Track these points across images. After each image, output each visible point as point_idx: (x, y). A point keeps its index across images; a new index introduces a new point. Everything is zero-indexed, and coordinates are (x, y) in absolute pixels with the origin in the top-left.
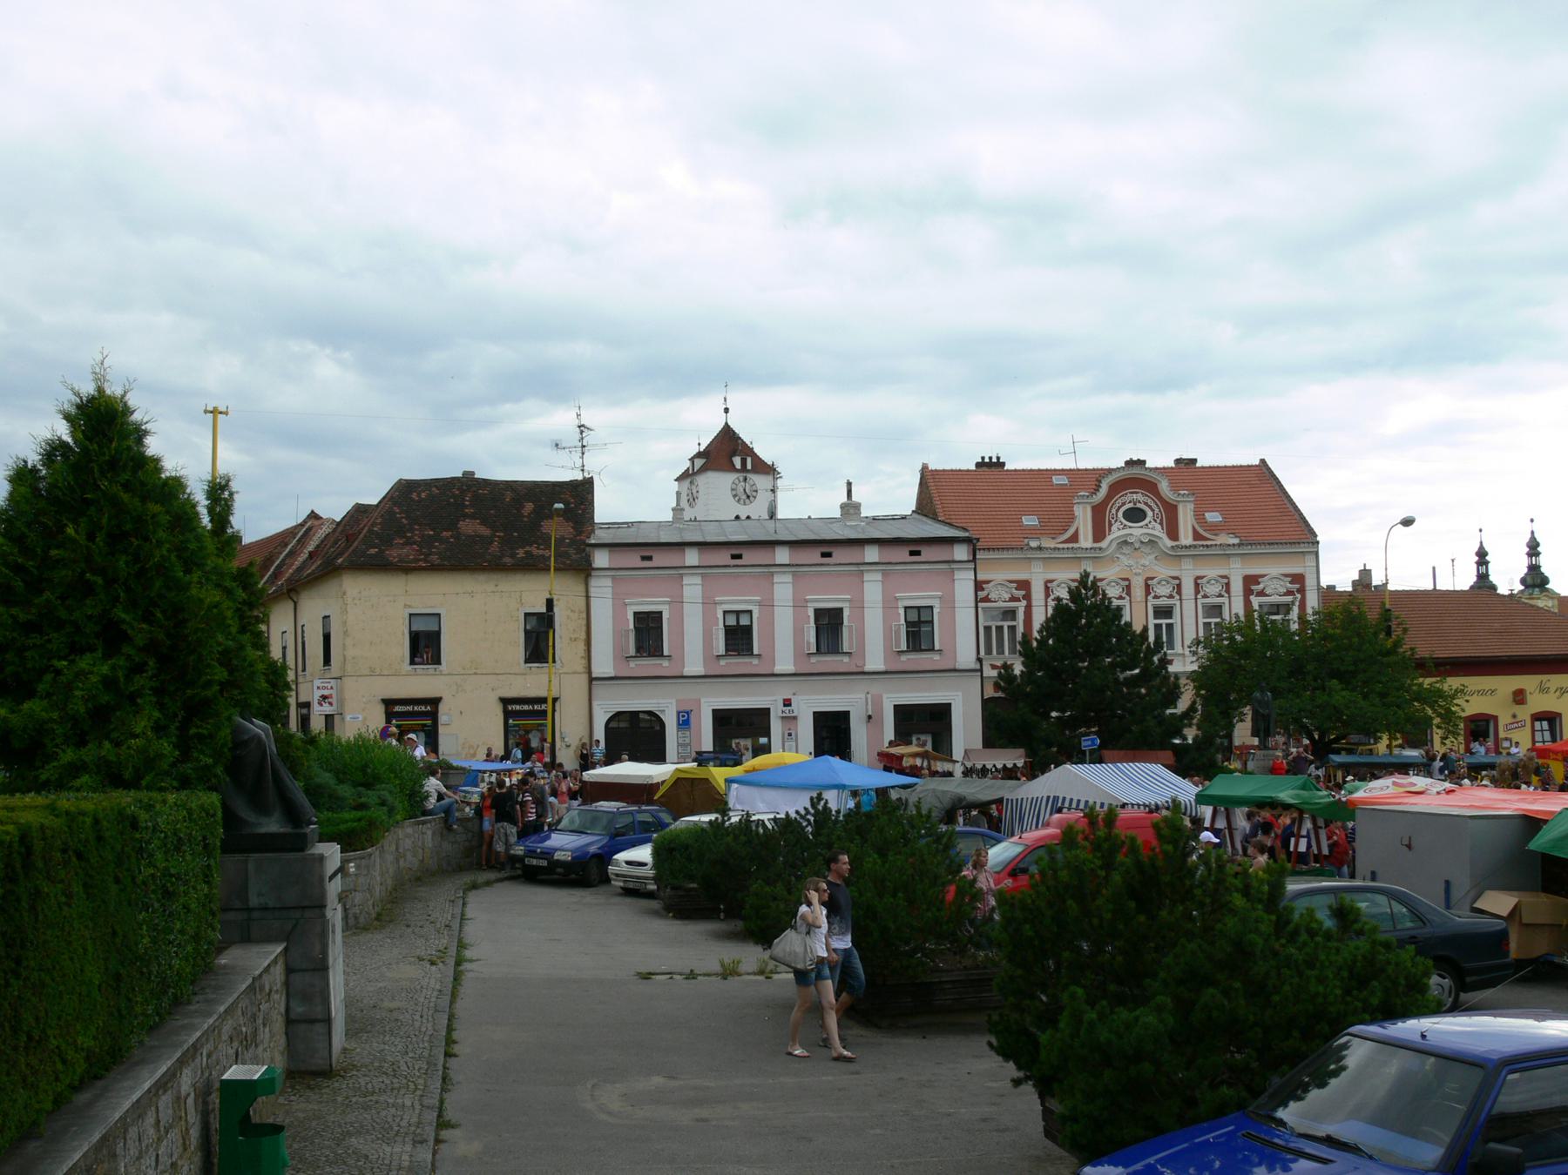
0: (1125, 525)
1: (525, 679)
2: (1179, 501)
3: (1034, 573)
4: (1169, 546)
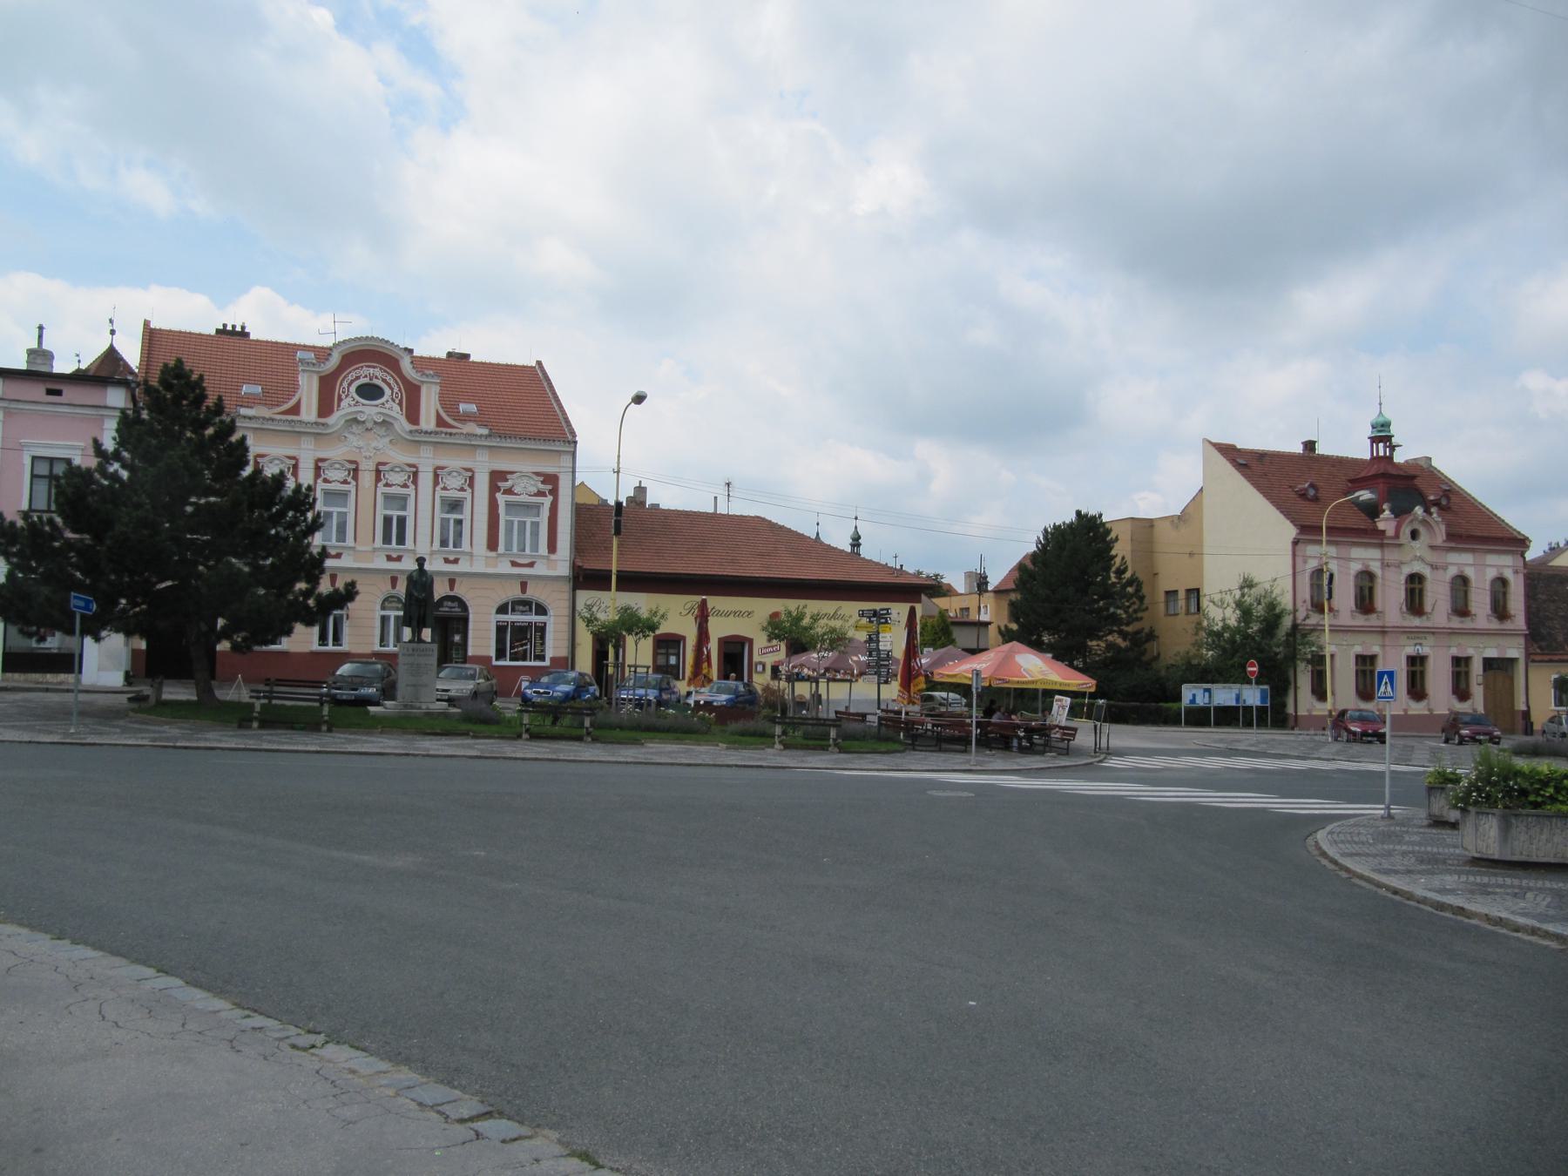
0: (357, 402)
2: (423, 382)
3: (423, 457)
4: (408, 430)
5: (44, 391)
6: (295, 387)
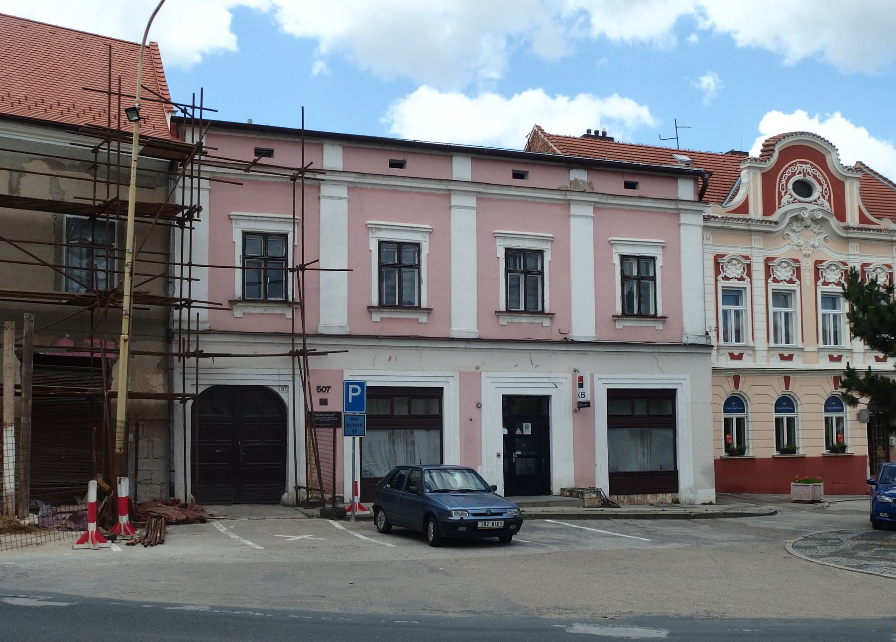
0: (795, 199)
1: (81, 271)
2: (846, 177)
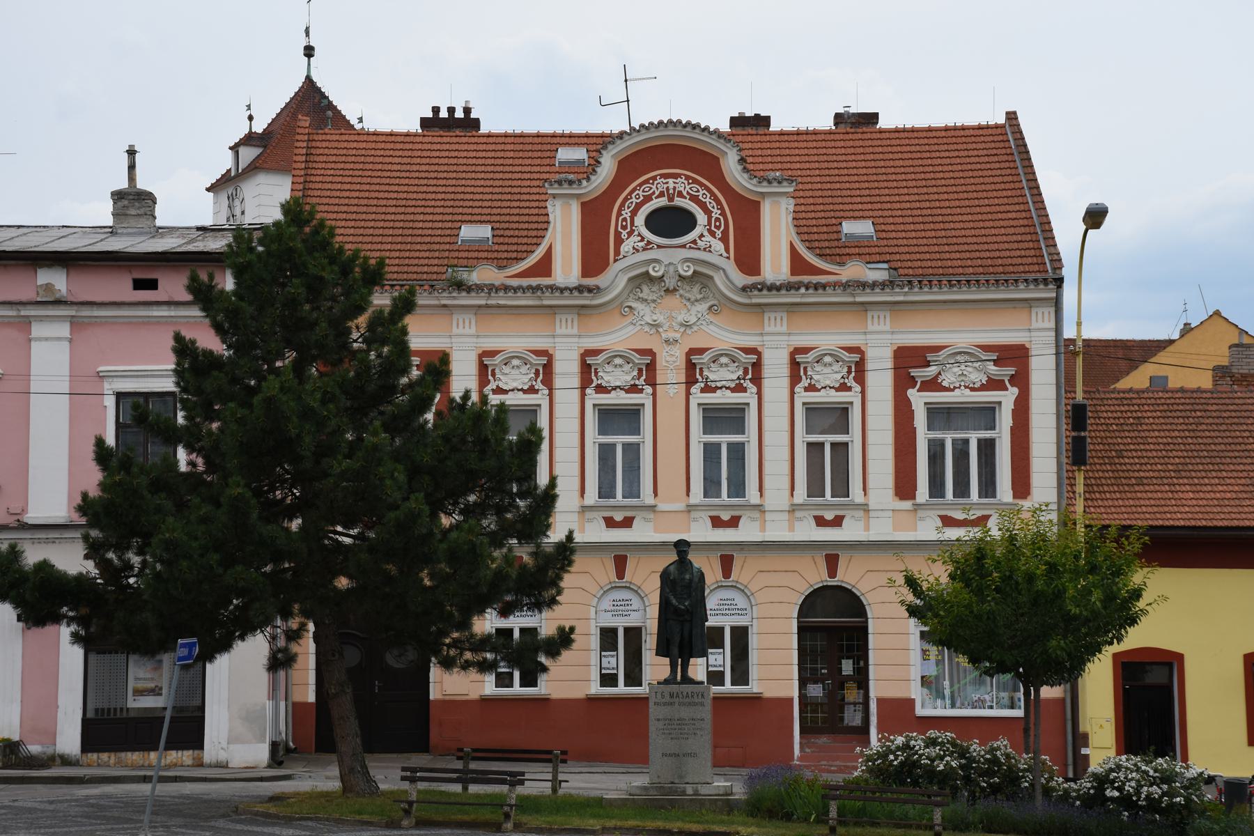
0: (649, 243)
2: (763, 195)
4: (740, 285)
5: (130, 284)
6: (543, 224)
